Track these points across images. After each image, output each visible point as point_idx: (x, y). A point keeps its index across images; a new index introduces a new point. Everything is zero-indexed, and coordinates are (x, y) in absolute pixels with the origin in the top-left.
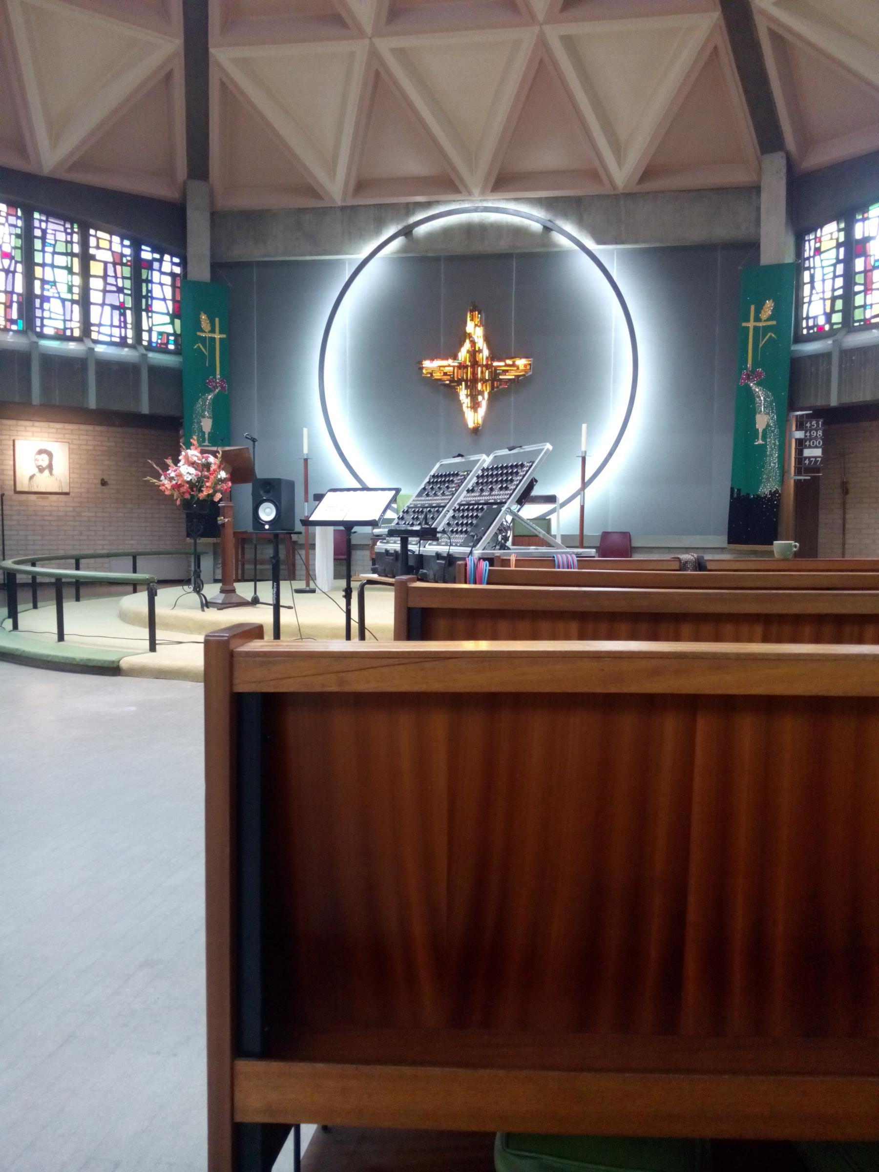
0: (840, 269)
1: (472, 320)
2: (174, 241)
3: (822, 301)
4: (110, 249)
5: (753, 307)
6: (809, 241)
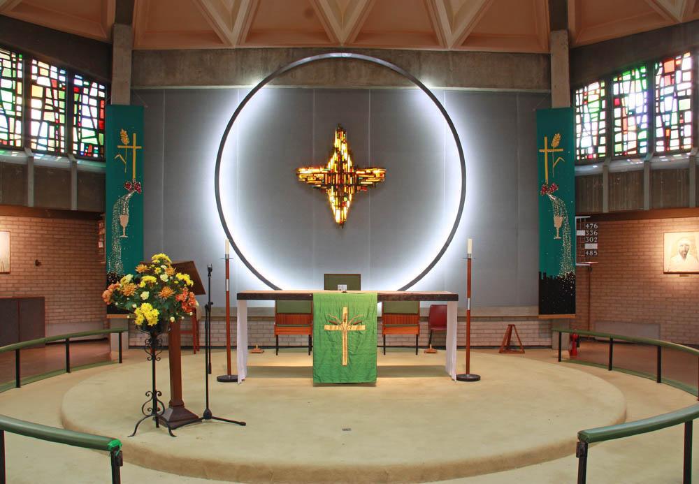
0: (603, 115)
1: (338, 138)
2: (102, 75)
3: (590, 137)
4: (49, 77)
5: (546, 139)
6: (579, 94)
